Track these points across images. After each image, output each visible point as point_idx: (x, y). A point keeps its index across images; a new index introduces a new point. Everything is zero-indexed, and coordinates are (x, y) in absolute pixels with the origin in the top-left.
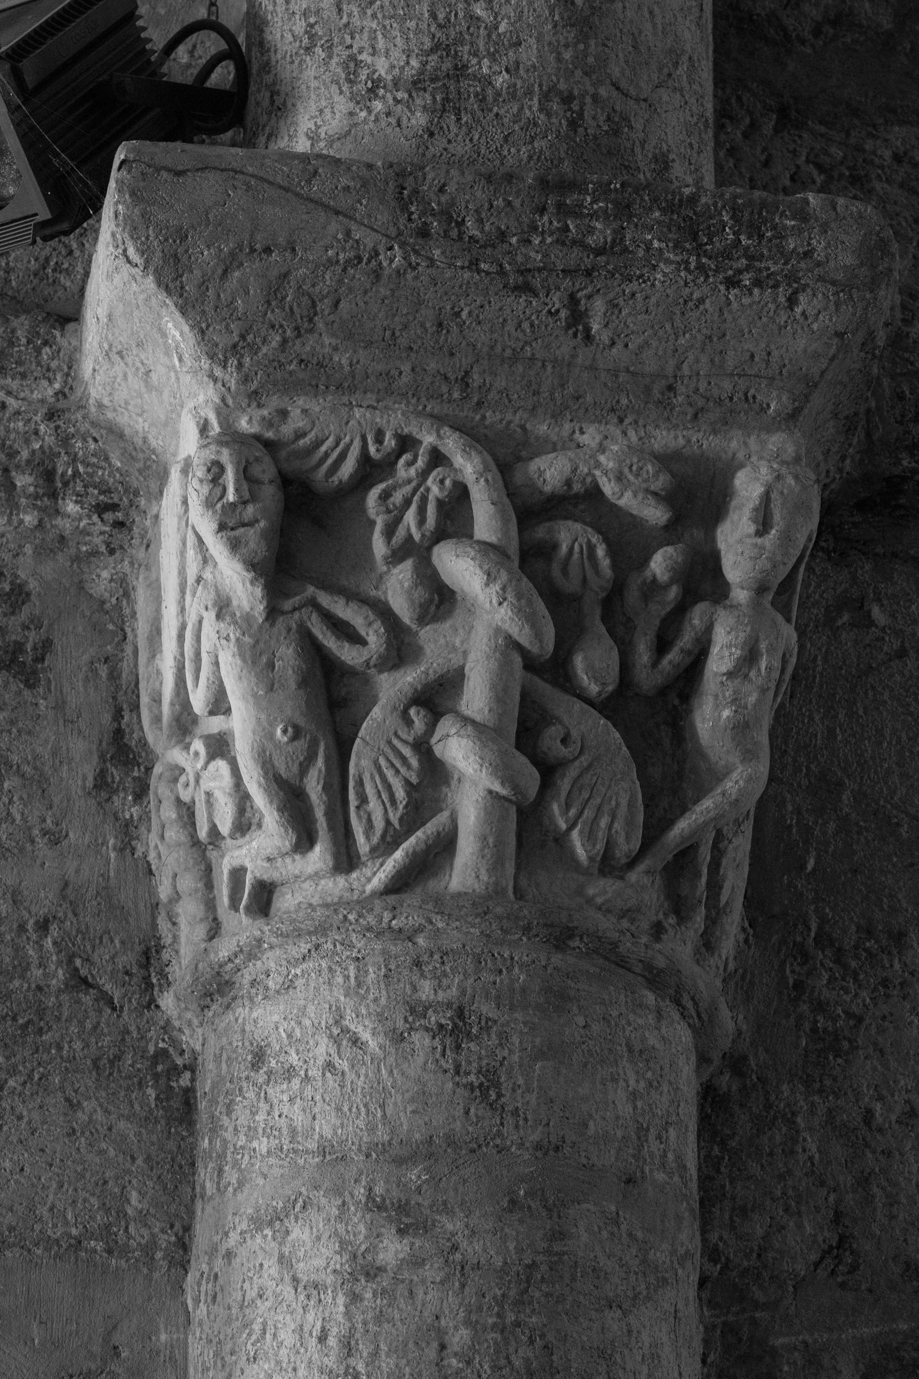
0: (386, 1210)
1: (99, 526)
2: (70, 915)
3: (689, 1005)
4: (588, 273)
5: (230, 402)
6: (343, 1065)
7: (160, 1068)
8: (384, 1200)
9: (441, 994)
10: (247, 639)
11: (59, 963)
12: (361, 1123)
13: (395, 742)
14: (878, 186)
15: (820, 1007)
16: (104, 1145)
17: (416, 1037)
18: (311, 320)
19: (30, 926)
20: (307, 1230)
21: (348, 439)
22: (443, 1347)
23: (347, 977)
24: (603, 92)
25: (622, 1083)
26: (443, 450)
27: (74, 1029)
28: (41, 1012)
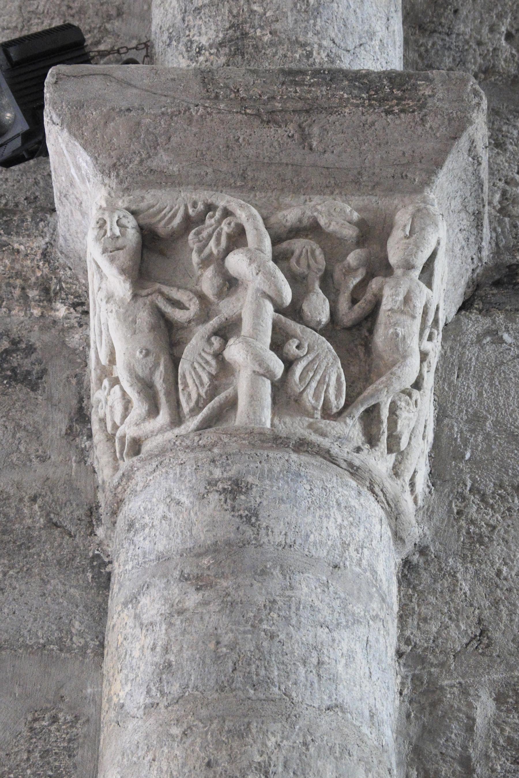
0: (190, 580)
1: (75, 314)
2: (49, 493)
3: (380, 494)
4: (307, 111)
5: (113, 195)
6: (171, 515)
7: (95, 563)
8: (189, 575)
9: (225, 473)
10: (121, 310)
11: (41, 516)
12: (178, 541)
13: (203, 354)
14: (510, 147)
15: (472, 522)
16: (61, 600)
17: (210, 496)
18: (155, 148)
19: (26, 499)
20: (148, 598)
21: (177, 207)
22: (218, 643)
23: (176, 474)
24: (325, 43)
25: (332, 519)
26: (230, 208)
27: (48, 546)
28: (30, 538)
